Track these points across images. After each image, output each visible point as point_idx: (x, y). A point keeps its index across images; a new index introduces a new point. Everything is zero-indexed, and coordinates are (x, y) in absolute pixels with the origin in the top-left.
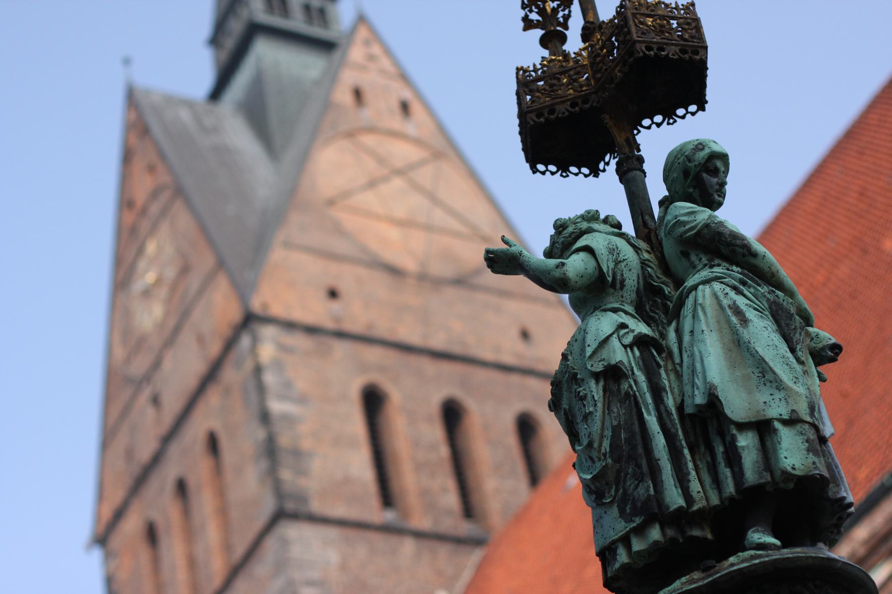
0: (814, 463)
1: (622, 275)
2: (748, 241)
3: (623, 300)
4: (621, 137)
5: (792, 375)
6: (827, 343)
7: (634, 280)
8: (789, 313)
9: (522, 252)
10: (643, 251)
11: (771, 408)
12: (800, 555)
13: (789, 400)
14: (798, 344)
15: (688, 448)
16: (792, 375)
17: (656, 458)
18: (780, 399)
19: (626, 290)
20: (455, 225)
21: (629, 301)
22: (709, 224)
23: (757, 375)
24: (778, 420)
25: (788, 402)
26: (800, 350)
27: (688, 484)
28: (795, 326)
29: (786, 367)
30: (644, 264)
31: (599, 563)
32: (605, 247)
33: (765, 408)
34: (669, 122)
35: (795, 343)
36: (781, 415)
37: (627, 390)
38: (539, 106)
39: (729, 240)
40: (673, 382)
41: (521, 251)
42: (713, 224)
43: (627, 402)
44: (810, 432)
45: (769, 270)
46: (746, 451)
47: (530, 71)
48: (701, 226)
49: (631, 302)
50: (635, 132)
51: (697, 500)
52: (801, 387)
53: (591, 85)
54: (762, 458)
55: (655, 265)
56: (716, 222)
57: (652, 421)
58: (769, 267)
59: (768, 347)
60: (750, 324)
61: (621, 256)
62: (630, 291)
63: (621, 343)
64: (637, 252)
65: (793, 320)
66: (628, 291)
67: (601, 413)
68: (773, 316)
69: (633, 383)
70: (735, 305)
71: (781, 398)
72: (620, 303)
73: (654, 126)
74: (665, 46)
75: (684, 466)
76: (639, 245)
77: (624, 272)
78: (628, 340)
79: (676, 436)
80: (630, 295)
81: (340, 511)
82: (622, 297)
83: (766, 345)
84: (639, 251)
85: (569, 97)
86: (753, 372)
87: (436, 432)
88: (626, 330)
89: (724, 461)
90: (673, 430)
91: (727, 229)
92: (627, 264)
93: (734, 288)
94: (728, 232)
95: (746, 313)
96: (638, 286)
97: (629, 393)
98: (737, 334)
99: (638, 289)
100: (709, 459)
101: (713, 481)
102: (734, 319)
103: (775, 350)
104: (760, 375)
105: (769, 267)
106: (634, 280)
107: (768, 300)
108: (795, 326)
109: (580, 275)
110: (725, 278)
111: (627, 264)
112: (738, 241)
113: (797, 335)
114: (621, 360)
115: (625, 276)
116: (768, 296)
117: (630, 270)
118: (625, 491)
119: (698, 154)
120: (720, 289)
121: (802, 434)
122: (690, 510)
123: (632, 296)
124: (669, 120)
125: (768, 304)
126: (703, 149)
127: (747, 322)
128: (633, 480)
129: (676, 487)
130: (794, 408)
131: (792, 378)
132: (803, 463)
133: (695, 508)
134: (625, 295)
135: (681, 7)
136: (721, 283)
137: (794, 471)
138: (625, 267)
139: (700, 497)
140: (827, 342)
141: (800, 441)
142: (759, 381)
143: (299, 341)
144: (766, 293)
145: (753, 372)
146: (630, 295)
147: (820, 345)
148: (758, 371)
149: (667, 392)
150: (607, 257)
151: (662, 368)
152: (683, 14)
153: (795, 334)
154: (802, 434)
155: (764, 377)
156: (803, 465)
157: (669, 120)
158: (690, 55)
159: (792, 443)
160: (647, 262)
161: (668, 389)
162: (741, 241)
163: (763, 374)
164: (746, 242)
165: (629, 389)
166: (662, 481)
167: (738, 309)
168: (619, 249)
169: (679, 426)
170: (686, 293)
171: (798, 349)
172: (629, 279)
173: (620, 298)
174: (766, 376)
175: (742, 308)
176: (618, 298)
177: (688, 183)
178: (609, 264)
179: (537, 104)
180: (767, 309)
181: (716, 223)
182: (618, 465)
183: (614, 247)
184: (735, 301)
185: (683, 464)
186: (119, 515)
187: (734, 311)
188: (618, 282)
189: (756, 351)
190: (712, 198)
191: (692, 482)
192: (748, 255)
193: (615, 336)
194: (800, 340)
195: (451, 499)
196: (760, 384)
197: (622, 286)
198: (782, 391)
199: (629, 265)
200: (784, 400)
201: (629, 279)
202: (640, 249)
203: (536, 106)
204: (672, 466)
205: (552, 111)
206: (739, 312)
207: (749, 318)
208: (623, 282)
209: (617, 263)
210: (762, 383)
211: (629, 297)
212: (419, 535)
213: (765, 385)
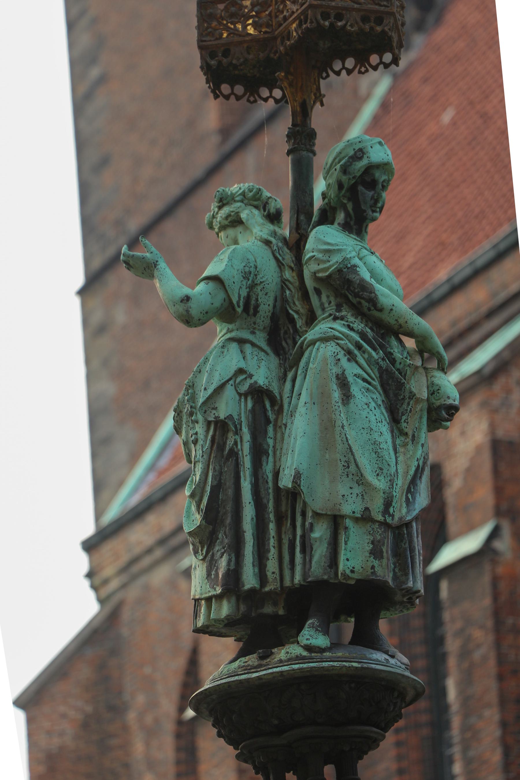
0: (373, 567)
1: (257, 300)
2: (376, 295)
3: (255, 326)
5: (377, 466)
6: (444, 403)
7: (269, 305)
8: (400, 382)
9: (158, 263)
10: (287, 268)
11: (347, 503)
12: (335, 664)
13: (365, 497)
14: (404, 415)
15: (276, 522)
16: (377, 466)
17: (243, 530)
18: (357, 494)
19: (260, 316)
21: (262, 328)
22: (341, 268)
23: (343, 462)
24: (350, 517)
25: (364, 499)
26: (405, 421)
27: (267, 561)
28: (404, 396)
29: (374, 455)
30: (284, 283)
32: (240, 271)
33: (342, 502)
34: (361, 70)
35: (400, 414)
36: (354, 512)
37: (232, 447)
38: (213, 43)
39: (356, 290)
40: (278, 442)
41: (157, 261)
42: (345, 268)
43: (231, 460)
44: (378, 532)
45: (395, 322)
46: (318, 543)
48: (332, 270)
49: (264, 328)
50: (324, 75)
51: (270, 581)
52: (383, 480)
53: (272, 25)
54: (330, 553)
55: (294, 287)
56: (349, 266)
57: (246, 486)
58: (397, 320)
59: (362, 430)
60: (352, 401)
61: (258, 277)
62: (264, 317)
63: (237, 391)
64: (280, 267)
65: (403, 389)
66: (262, 317)
67: (206, 466)
68: (382, 386)
69: (239, 440)
70: (343, 375)
71: (359, 494)
72: (252, 330)
74: (344, 12)
75: (267, 541)
76: (283, 259)
77: (259, 297)
78: (244, 388)
79: (267, 507)
80: (263, 321)
82: (255, 323)
83: (361, 427)
84: (282, 267)
86: (340, 459)
88: (244, 376)
89: (300, 545)
90: (265, 501)
91: (358, 277)
92: (264, 288)
93: (349, 352)
94: (358, 281)
95: (351, 386)
96: (273, 311)
97: (234, 450)
98: (335, 414)
99: (273, 314)
100: (291, 536)
101: (290, 561)
102: (336, 395)
103: (368, 434)
104: (346, 464)
105: (397, 320)
106: (269, 305)
107: (380, 368)
108: (404, 396)
109: (204, 312)
110: (341, 339)
111: (264, 288)
112: (365, 293)
113: (405, 406)
114: (230, 415)
115: (260, 300)
116: (381, 363)
117: (266, 294)
118: (213, 554)
119: (355, 165)
120: (334, 352)
121: (370, 534)
122: (263, 590)
123: (265, 322)
124: (360, 68)
125: (379, 373)
126: (361, 158)
127: (350, 398)
128: (221, 547)
129: (253, 566)
130: (368, 506)
131: (376, 469)
132: (363, 566)
133: (267, 589)
134: (258, 321)
136: (338, 344)
137: (353, 574)
138: (261, 290)
139: (273, 578)
140: (445, 401)
141: (367, 541)
142: (344, 471)
144: (380, 360)
145: (340, 459)
146: (263, 321)
147: (438, 403)
148: (344, 459)
149: (269, 455)
150: (240, 284)
151: (271, 425)
153: (402, 404)
154: (370, 534)
155: (348, 467)
156: (362, 568)
157: (360, 68)
159: (359, 542)
160: (287, 283)
161: (271, 452)
162: (368, 294)
163: (348, 464)
164: (373, 295)
165: (235, 447)
166: (244, 555)
167: (345, 380)
168: (258, 269)
169: (271, 497)
170: (306, 345)
171: (403, 421)
172: (264, 304)
173: (252, 325)
174: (350, 468)
175: (349, 380)
176: (251, 325)
177: (341, 194)
178: (241, 293)
179: (212, 39)
180: (377, 378)
181: (348, 268)
182: (211, 527)
183: (252, 269)
184: (345, 370)
185: (267, 540)
187: (341, 382)
188: (252, 307)
189: (347, 438)
190: (365, 214)
191: (270, 560)
192: (373, 310)
193: (231, 382)
194: (407, 410)
196: (343, 474)
197: (256, 312)
198: (361, 486)
199: (265, 289)
200: (361, 497)
201: (264, 304)
202: (283, 265)
203: (210, 41)
204: (256, 542)
205: (226, 53)
206: (345, 384)
207: (354, 393)
208: (257, 306)
209: (252, 287)
210: (346, 473)
211: (261, 323)
213: (348, 477)
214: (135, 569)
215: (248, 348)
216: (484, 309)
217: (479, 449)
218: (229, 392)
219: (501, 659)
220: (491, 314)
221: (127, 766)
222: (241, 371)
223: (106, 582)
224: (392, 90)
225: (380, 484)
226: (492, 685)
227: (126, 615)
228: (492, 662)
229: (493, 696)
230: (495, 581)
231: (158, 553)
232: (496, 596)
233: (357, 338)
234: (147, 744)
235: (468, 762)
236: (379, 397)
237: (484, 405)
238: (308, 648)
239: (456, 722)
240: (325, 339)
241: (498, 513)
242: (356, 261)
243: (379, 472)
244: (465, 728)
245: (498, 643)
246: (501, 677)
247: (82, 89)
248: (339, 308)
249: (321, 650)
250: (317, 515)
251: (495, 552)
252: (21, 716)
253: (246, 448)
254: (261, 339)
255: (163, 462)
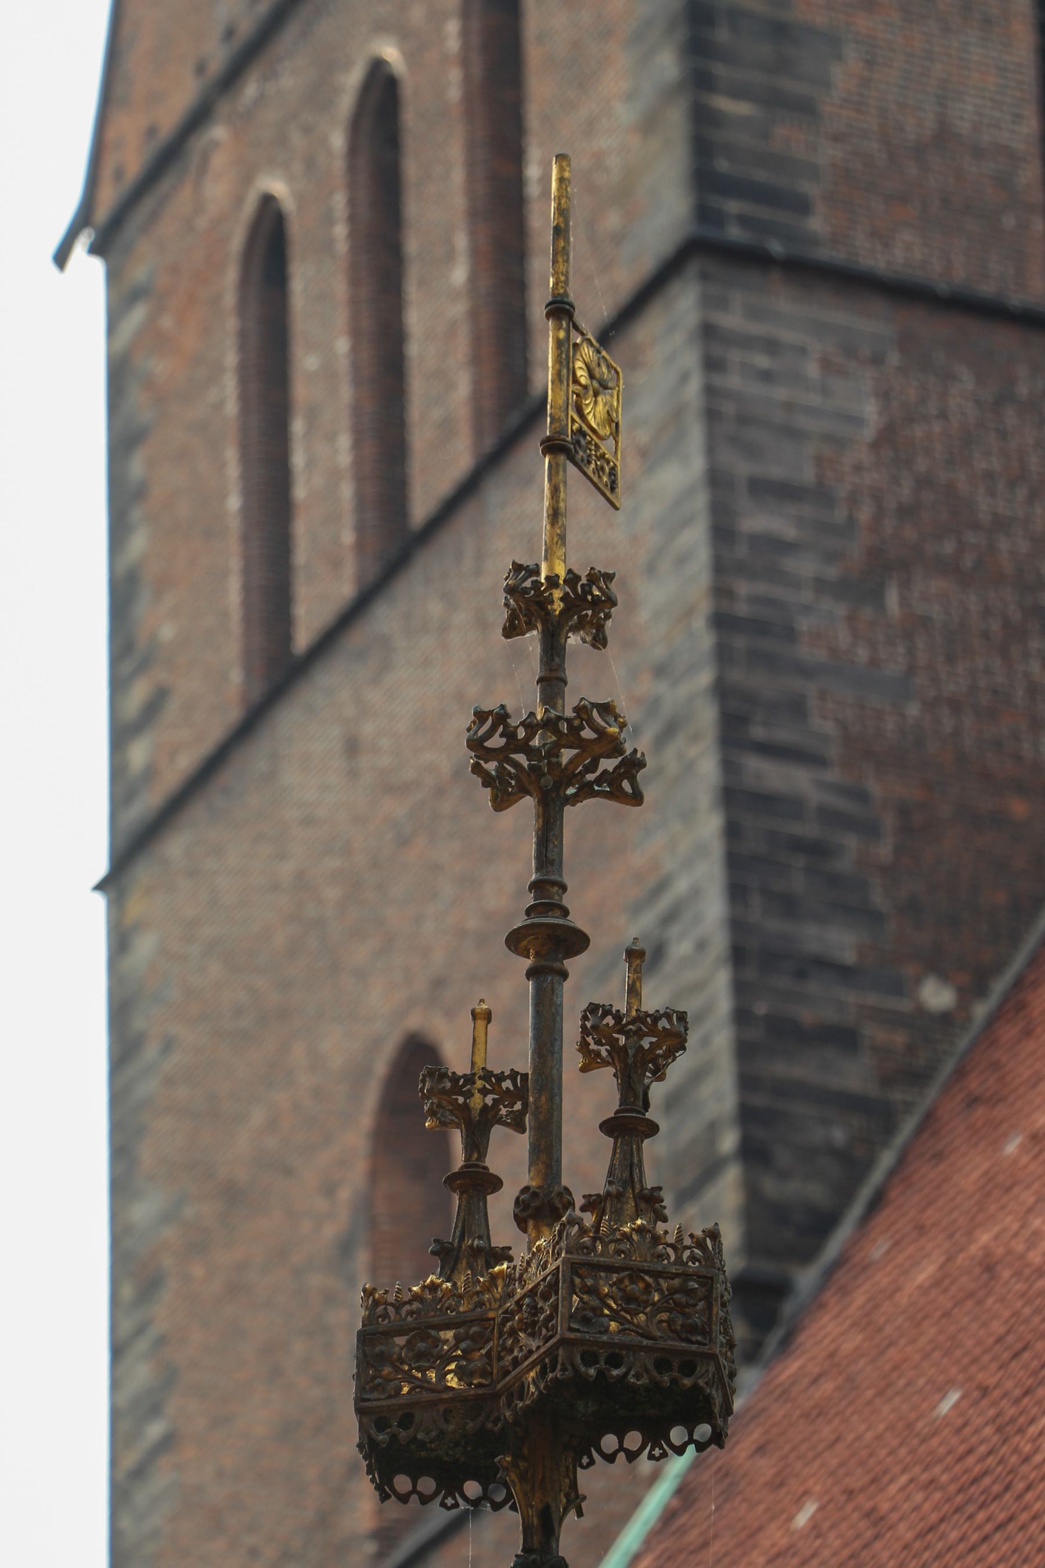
4: (532, 1507)
20: (593, 410)
38: (384, 1403)
47: (386, 1303)
53: (492, 1373)
85: (445, 1396)
124: (652, 1449)
135: (688, 1242)
157: (652, 1449)
158: (676, 1374)
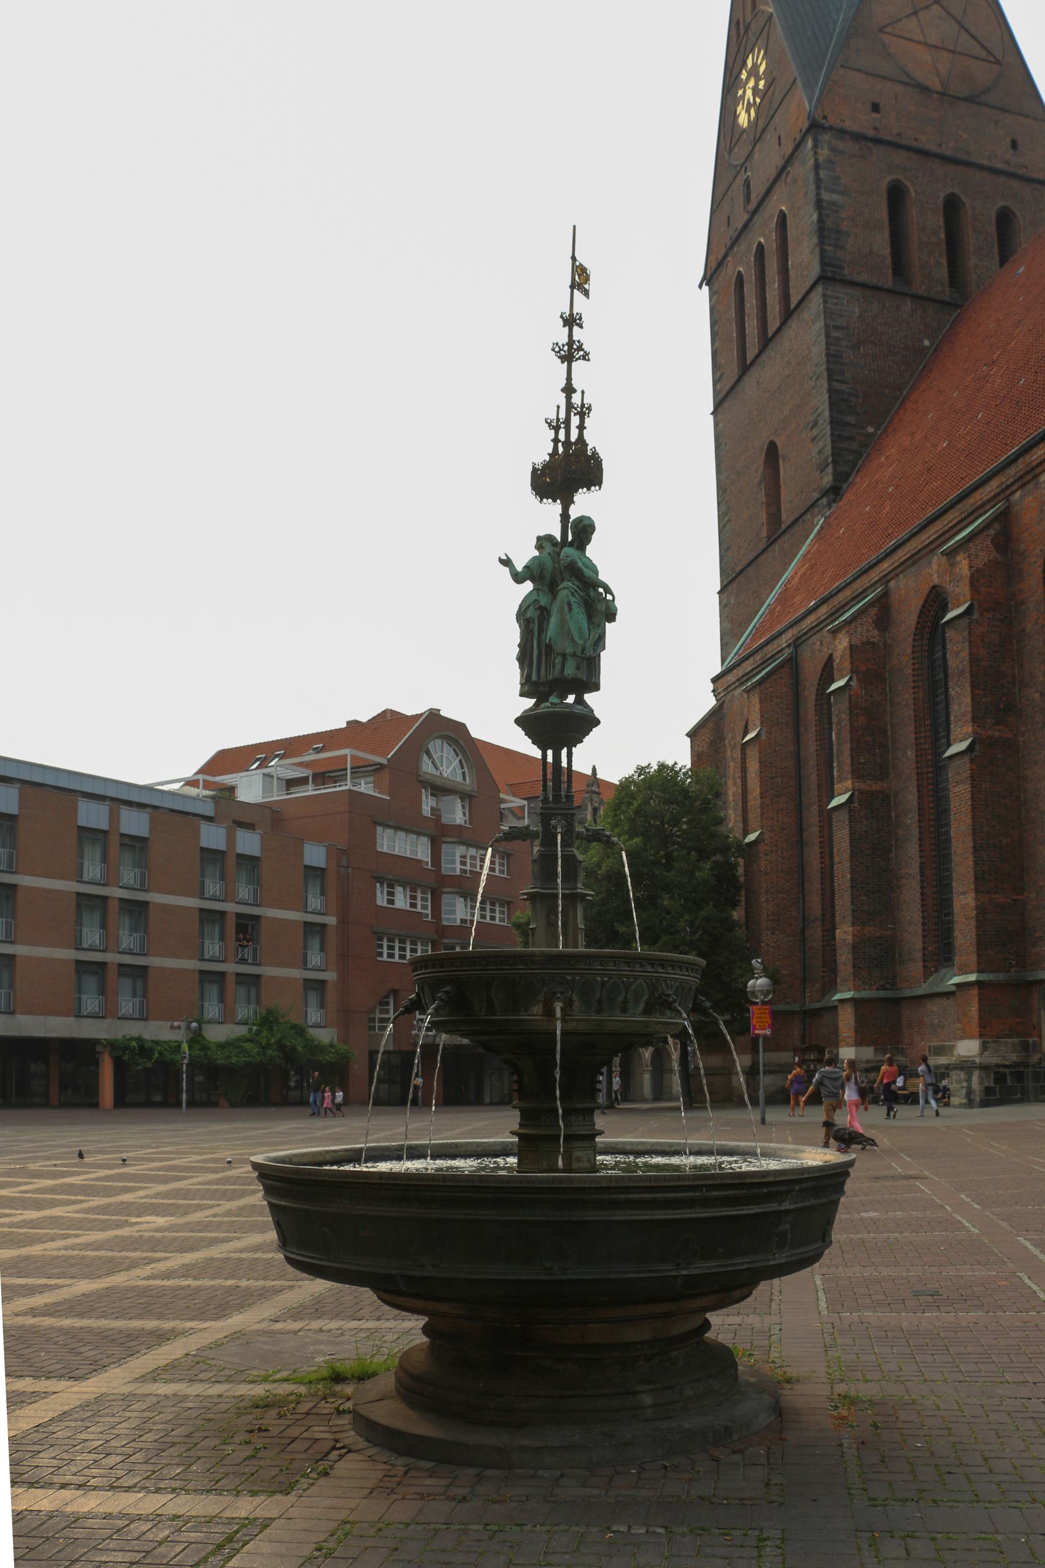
20: (976, 50)
30: (555, 568)
31: (763, 1286)
73: (560, 344)
81: (863, 278)
87: (938, 221)
102: (566, 609)
143: (847, 146)
152: (662, 857)
186: (720, 264)
195: (943, 272)
212: (915, 297)
214: (729, 689)
215: (540, 592)
216: (850, 598)
217: (845, 648)
218: (531, 608)
219: (852, 726)
220: (852, 600)
221: (725, 759)
222: (535, 600)
223: (719, 693)
224: (824, 522)
225: (580, 642)
226: (848, 734)
227: (726, 706)
228: (848, 727)
229: (848, 739)
230: (850, 696)
231: (737, 684)
232: (850, 703)
233: (575, 587)
234: (732, 752)
235: (839, 762)
236: (583, 610)
237: (847, 632)
238: (552, 703)
239: (835, 748)
240: (565, 588)
241: (852, 672)
242: (578, 560)
243: (581, 637)
244: (839, 750)
245: (851, 720)
246: (851, 732)
247: (722, 524)
248: (571, 577)
249: (556, 704)
250: (558, 654)
251: (851, 686)
252: (689, 739)
253: (536, 628)
254: (546, 589)
255: (741, 652)
